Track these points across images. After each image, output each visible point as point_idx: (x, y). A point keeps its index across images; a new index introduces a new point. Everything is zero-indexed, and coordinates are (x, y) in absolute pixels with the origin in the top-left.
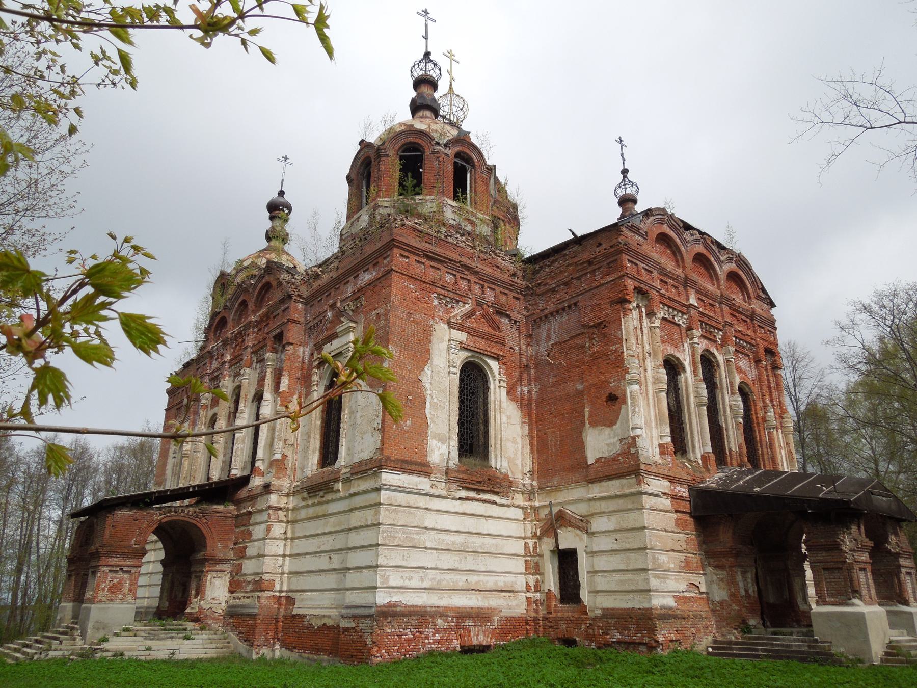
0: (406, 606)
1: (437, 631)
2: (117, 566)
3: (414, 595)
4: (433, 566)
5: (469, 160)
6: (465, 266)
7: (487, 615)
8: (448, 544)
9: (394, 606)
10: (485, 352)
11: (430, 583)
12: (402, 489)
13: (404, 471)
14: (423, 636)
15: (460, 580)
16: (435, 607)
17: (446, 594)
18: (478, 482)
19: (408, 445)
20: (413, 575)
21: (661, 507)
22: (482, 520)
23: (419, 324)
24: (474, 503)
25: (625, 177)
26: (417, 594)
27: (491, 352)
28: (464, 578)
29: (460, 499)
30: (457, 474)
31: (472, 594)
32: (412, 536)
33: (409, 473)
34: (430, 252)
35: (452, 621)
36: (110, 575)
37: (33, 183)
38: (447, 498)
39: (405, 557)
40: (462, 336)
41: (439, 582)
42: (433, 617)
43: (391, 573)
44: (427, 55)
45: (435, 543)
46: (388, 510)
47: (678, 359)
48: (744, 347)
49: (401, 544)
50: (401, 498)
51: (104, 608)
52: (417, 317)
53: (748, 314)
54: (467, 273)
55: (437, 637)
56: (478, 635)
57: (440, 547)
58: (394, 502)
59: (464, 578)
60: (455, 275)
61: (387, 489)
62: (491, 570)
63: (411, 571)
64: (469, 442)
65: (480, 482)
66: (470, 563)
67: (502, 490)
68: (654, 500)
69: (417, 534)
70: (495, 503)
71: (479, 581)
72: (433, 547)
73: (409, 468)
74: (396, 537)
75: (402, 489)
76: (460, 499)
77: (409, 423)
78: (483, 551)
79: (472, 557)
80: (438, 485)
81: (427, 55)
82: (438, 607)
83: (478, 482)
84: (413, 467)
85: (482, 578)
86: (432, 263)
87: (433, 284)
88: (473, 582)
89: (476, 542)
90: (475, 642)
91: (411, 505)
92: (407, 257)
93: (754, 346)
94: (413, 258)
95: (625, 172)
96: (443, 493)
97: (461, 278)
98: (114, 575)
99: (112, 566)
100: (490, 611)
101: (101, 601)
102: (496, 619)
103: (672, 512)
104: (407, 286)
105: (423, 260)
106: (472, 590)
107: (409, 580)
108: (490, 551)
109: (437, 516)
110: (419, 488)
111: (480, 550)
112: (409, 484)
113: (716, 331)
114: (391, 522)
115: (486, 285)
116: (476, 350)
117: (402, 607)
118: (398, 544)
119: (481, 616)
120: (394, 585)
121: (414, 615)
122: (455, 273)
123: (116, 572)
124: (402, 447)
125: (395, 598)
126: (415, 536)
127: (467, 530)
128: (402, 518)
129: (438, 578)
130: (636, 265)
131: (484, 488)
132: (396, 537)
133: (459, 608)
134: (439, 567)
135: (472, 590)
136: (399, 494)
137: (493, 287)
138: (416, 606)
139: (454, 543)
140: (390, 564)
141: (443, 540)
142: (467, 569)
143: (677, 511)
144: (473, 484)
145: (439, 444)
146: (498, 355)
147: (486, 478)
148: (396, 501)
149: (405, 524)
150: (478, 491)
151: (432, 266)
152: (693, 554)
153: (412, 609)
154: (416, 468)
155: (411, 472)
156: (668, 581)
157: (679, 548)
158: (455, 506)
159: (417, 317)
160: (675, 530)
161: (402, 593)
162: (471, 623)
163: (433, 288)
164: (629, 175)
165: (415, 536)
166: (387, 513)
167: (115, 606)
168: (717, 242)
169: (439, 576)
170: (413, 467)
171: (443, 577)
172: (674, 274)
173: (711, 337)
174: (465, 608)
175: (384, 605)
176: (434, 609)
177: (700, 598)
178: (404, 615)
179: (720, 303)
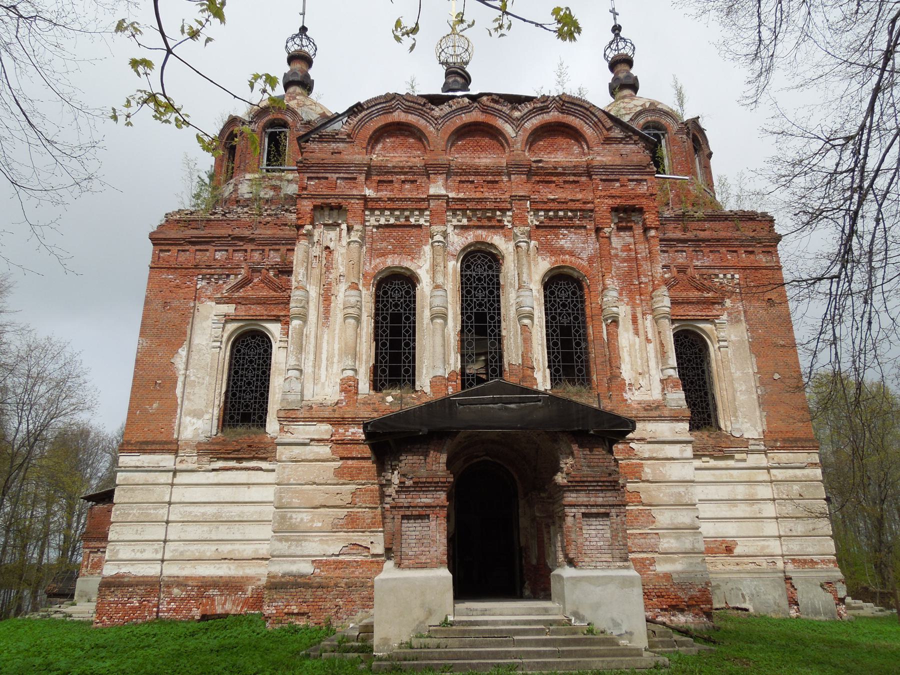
0: (135, 577)
1: (173, 600)
2: (95, 548)
3: (145, 566)
4: (176, 538)
5: (285, 125)
6: (237, 237)
7: (238, 584)
8: (196, 516)
9: (123, 576)
10: (262, 318)
11: (172, 554)
12: (139, 469)
13: (144, 452)
14: (151, 604)
15: (209, 550)
16: (174, 577)
17: (189, 565)
18: (235, 451)
19: (151, 427)
20: (146, 548)
21: (311, 457)
22: (245, 488)
23: (175, 310)
24: (235, 472)
25: (617, 35)
26: (149, 565)
27: (268, 316)
28: (214, 548)
29: (214, 470)
30: (207, 447)
31: (222, 563)
32: (149, 511)
33: (150, 453)
34: (192, 237)
35: (192, 590)
36: (92, 555)
37: (632, 227)
38: (199, 471)
39: (139, 532)
40: (229, 309)
41: (182, 553)
42: (168, 586)
43: (122, 547)
44: (303, 29)
45: (180, 516)
46: (123, 490)
47: (407, 269)
48: (571, 219)
49: (135, 519)
50: (139, 477)
51: (86, 580)
52: (175, 303)
53: (581, 170)
54: (241, 243)
55: (173, 605)
56: (225, 604)
57: (186, 520)
58: (131, 482)
59: (214, 548)
60: (227, 251)
61: (122, 471)
62: (250, 538)
63: (144, 544)
64: (241, 411)
65: (238, 451)
66: (223, 532)
67: (269, 455)
68: (296, 451)
69: (155, 509)
70: (261, 469)
71: (233, 550)
72: (178, 519)
73: (149, 448)
74: (130, 514)
75: (139, 469)
76: (214, 470)
77: (155, 406)
78: (241, 519)
79: (227, 527)
80: (189, 459)
81: (303, 29)
82: (178, 577)
83: (235, 451)
84: (153, 447)
85: (237, 546)
86: (198, 247)
87: (196, 267)
88: (226, 552)
89: (234, 511)
90: (219, 610)
91: (150, 482)
92: (169, 251)
93: (592, 211)
94: (175, 249)
95: (617, 29)
96: (195, 466)
97: (234, 251)
98: (95, 555)
99: (92, 548)
100: (245, 579)
101: (84, 575)
102: (250, 588)
103: (334, 460)
104: (165, 278)
105: (187, 248)
106: (225, 559)
107: (141, 552)
108: (252, 519)
109: (186, 489)
110: (160, 465)
111: (237, 519)
112: (149, 463)
113: (498, 213)
114: (127, 500)
115: (267, 248)
116: (247, 318)
117: (130, 577)
118: (132, 520)
119: (230, 586)
120: (124, 557)
121: (141, 586)
122: (226, 248)
123: (96, 552)
124: (146, 429)
125: (124, 570)
126: (152, 511)
127: (222, 500)
128: (139, 496)
129: (182, 549)
130: (327, 178)
131: (244, 456)
132: (130, 514)
133: (204, 577)
134: (182, 538)
135: (225, 559)
136: (136, 474)
137: (277, 247)
138: (147, 577)
139: (203, 514)
140: (121, 539)
141: (191, 513)
142: (218, 538)
143: (342, 459)
144: (229, 454)
145: (195, 420)
146: (279, 316)
147: (245, 446)
148: (134, 480)
149: (142, 501)
150: (239, 460)
151: (197, 250)
152: (370, 508)
153: (141, 579)
154: (158, 447)
155: (153, 452)
156: (304, 544)
157: (339, 503)
158: (208, 478)
159: (175, 303)
160: (335, 482)
161: (132, 565)
162: (216, 592)
163: (197, 271)
164: (622, 34)
165: (152, 511)
166: (122, 492)
167: (94, 578)
168: (501, 96)
169: (181, 547)
170: (153, 447)
171: (186, 548)
172: (403, 168)
173: (494, 223)
174: (212, 577)
175: (112, 577)
176: (172, 579)
177: (372, 562)
178: (130, 585)
179: (509, 175)
